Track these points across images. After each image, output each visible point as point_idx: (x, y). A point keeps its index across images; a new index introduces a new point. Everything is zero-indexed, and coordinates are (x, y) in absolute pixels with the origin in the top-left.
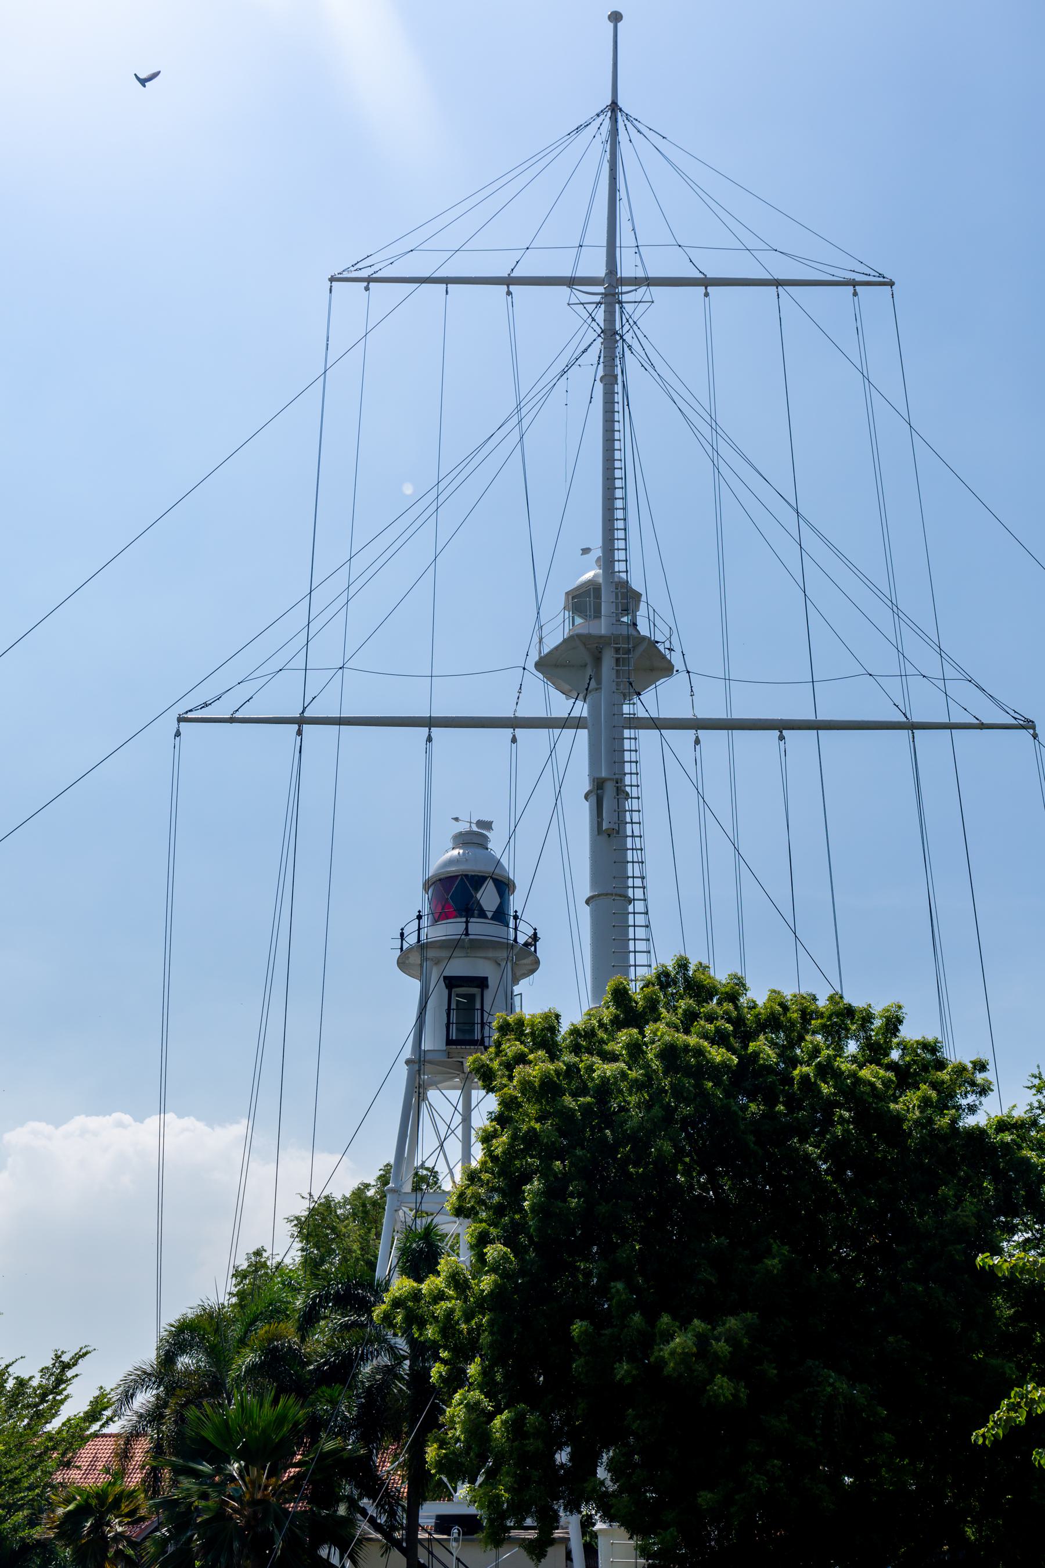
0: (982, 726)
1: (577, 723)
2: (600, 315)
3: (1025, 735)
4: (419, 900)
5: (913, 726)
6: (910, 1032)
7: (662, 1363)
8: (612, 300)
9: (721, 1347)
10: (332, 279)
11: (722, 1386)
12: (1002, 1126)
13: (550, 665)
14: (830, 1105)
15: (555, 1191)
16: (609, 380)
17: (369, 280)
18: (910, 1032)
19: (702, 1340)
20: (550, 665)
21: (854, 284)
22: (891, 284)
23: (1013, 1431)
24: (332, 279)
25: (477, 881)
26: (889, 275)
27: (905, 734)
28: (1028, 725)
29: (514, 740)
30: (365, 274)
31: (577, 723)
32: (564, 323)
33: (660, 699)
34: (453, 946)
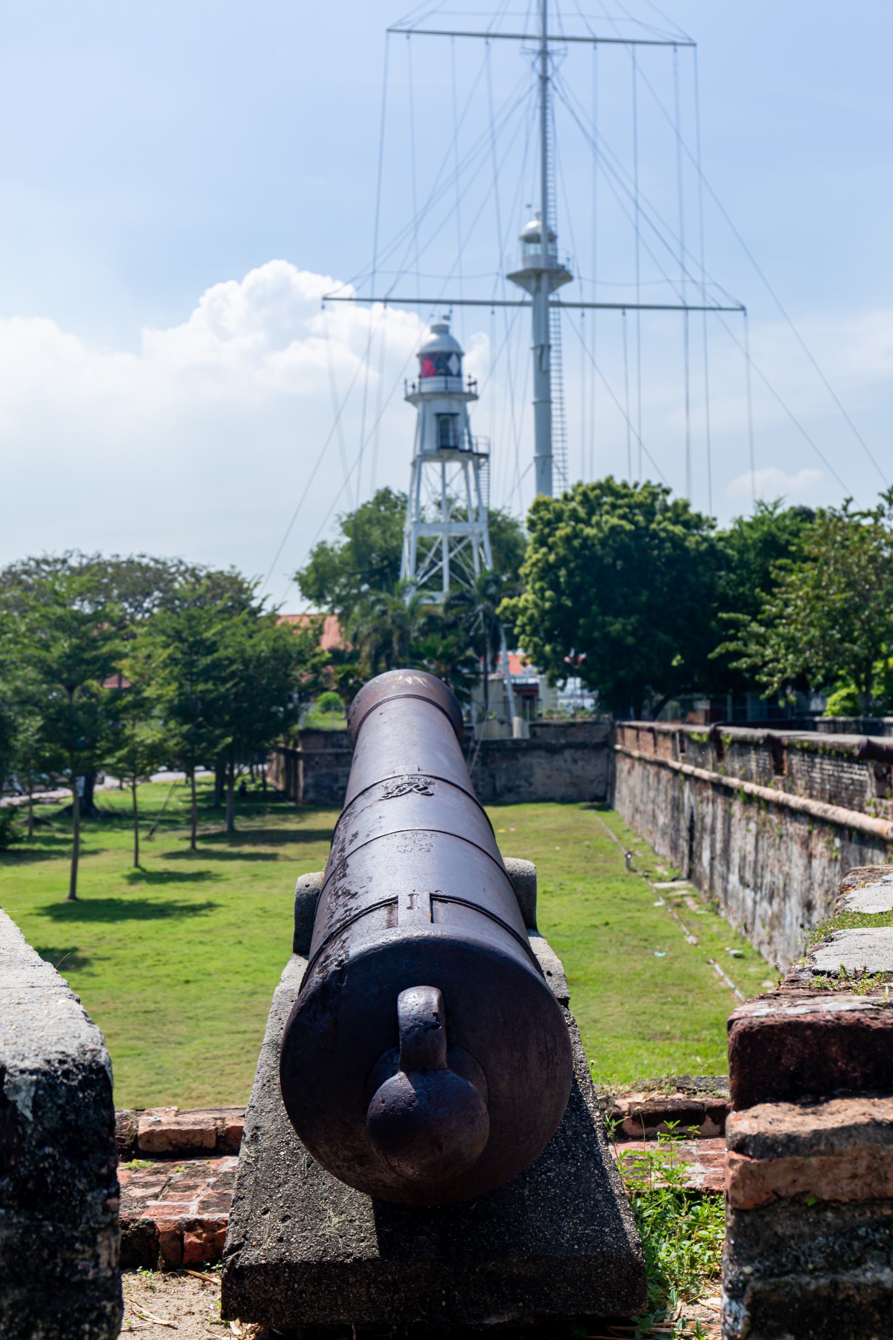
0: (720, 309)
1: (522, 304)
2: (538, 65)
3: (741, 313)
4: (415, 367)
5: (686, 308)
6: (693, 510)
7: (609, 632)
8: (544, 54)
9: (629, 627)
10: (389, 30)
11: (630, 640)
12: (720, 539)
13: (515, 278)
14: (662, 541)
15: (570, 574)
16: (544, 108)
17: (409, 32)
18: (693, 510)
19: (624, 625)
20: (515, 278)
21: (674, 44)
22: (694, 45)
23: (721, 655)
24: (389, 30)
25: (448, 356)
26: (695, 40)
27: (681, 313)
28: (743, 309)
29: (493, 313)
30: (406, 27)
31: (522, 304)
32: (515, 65)
33: (565, 293)
34: (436, 394)
